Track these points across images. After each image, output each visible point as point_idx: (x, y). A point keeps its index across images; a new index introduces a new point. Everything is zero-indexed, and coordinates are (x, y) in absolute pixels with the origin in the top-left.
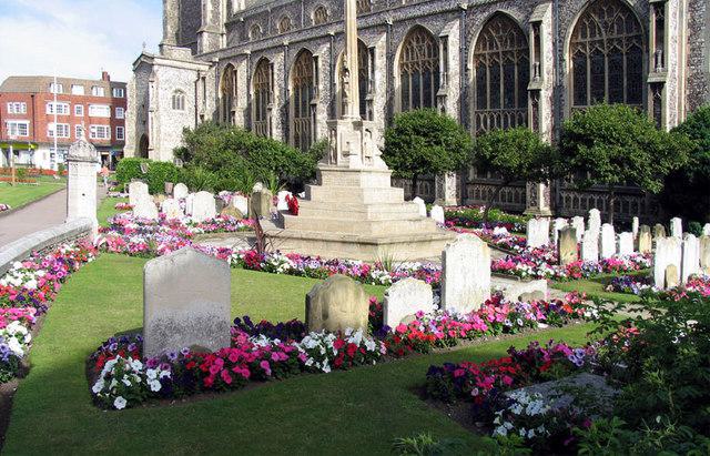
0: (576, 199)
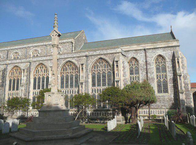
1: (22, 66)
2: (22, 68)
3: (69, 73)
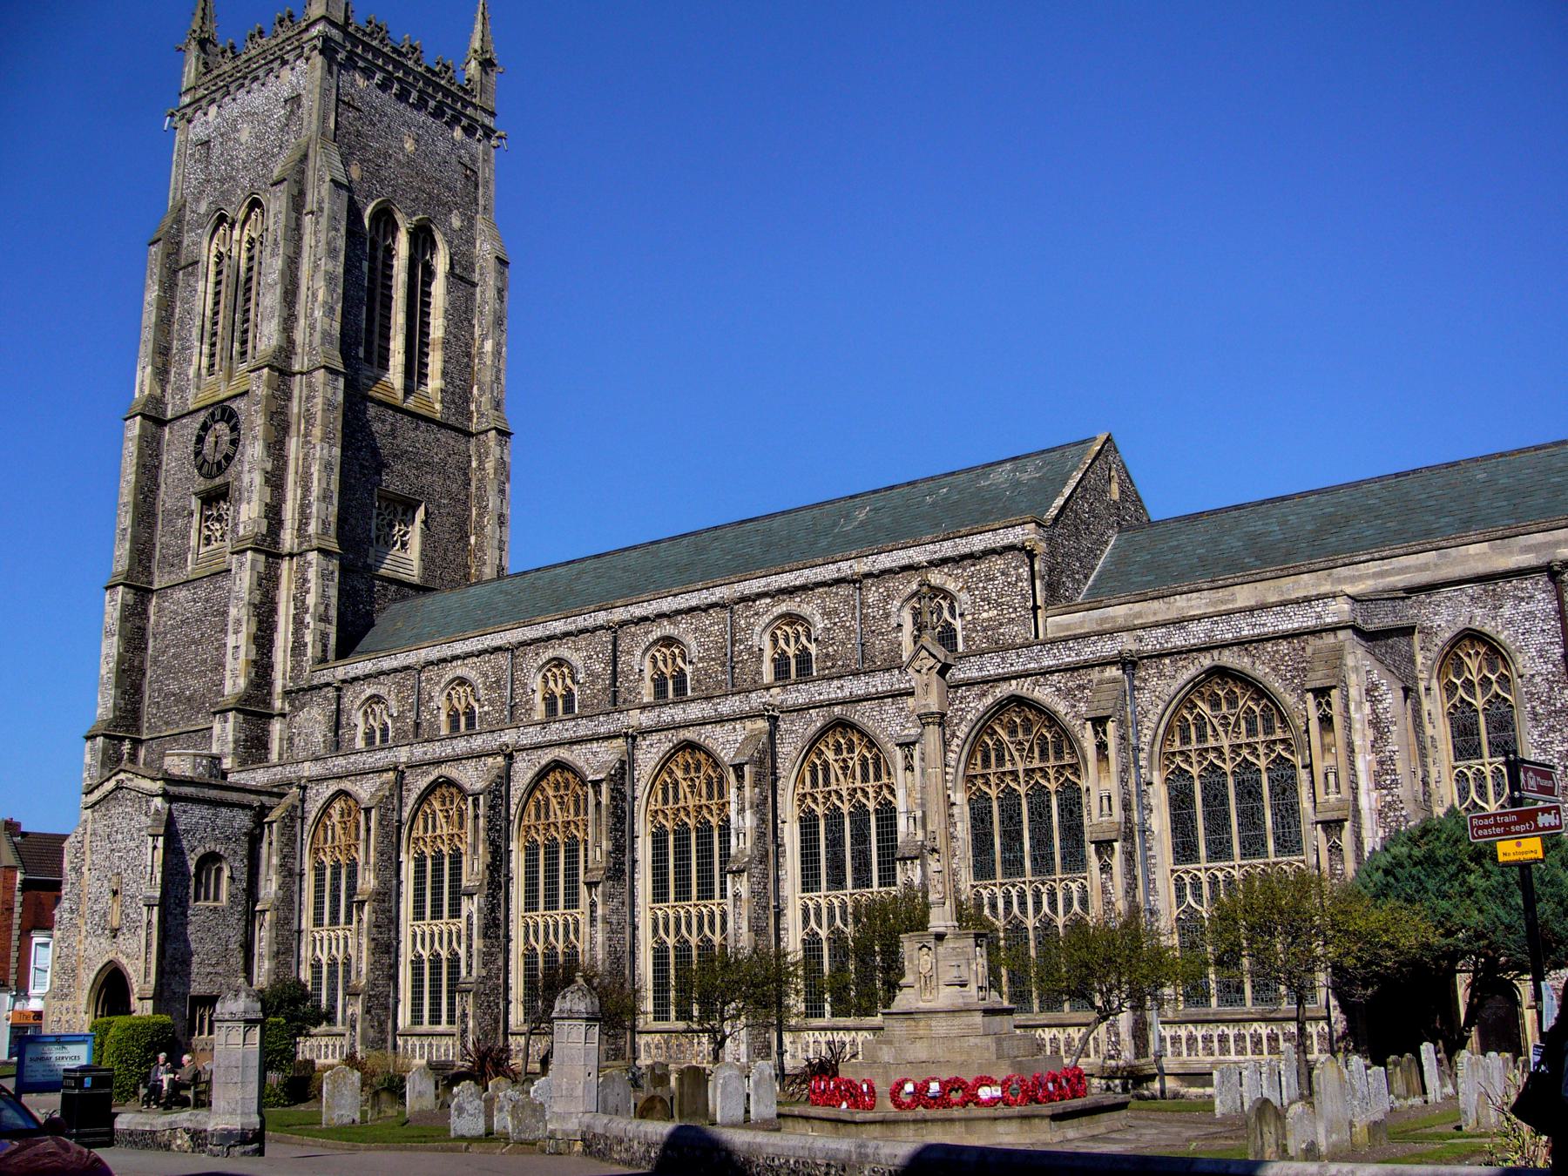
0: (1240, 1038)
1: (727, 743)
2: (727, 755)
3: (1021, 775)
